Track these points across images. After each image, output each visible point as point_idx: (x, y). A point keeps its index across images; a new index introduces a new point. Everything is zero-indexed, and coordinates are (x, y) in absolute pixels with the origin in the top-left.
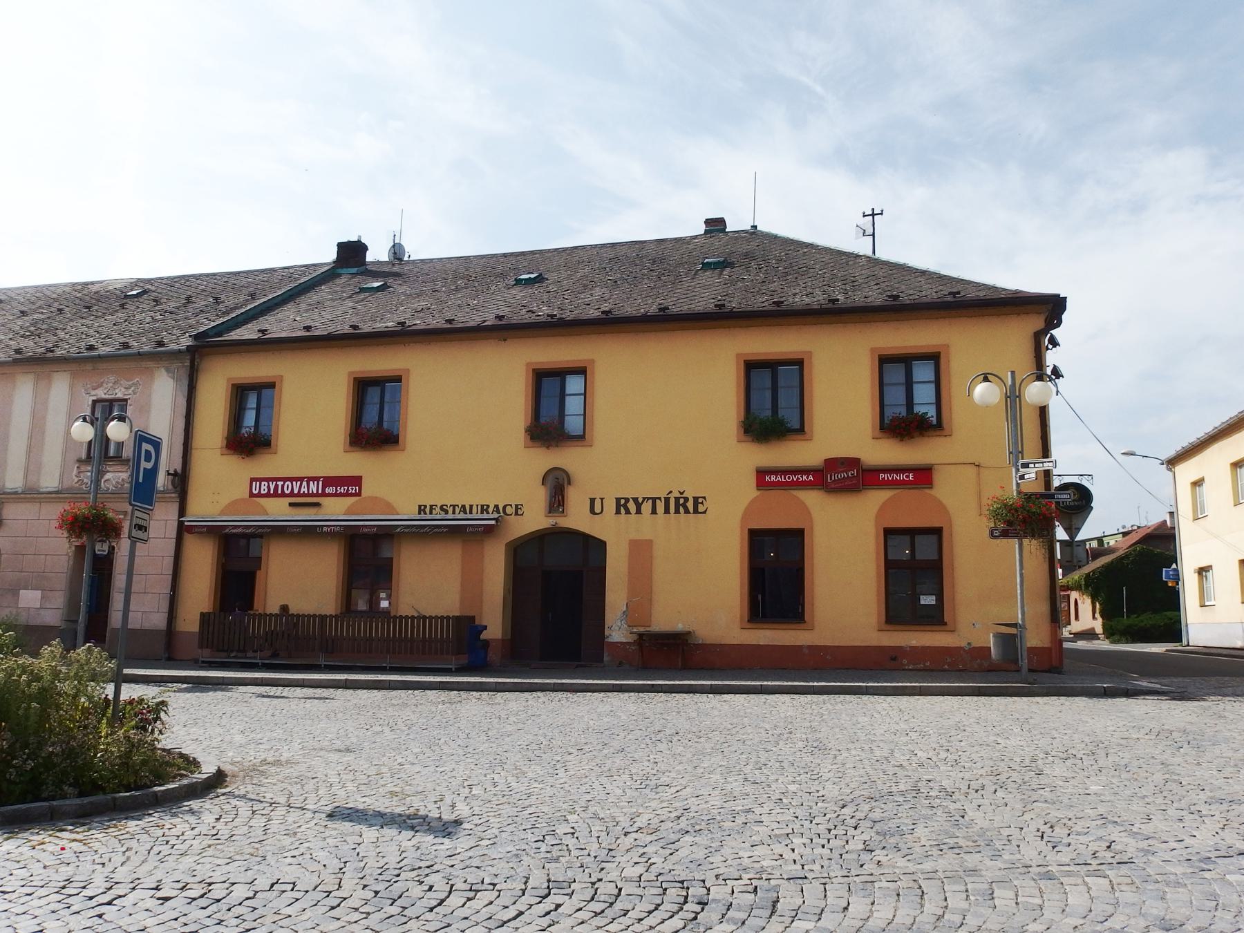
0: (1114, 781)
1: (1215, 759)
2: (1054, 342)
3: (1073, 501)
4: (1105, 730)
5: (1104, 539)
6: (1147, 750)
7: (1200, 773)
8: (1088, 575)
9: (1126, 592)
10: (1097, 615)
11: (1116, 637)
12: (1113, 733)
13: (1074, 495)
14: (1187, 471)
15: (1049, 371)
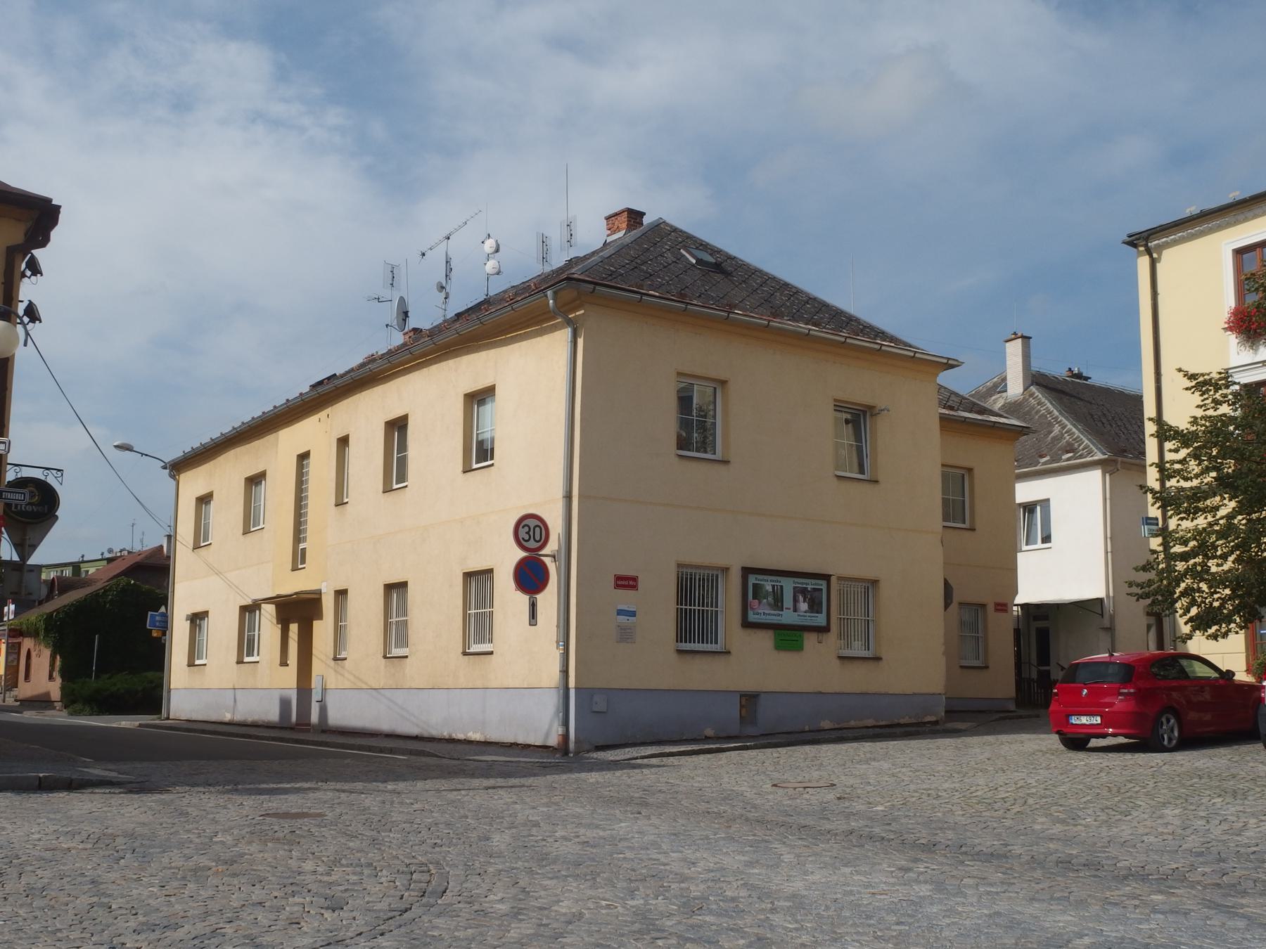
0: (21, 912)
1: (161, 871)
2: (35, 269)
3: (29, 504)
4: (26, 838)
5: (82, 565)
6: (76, 865)
7: (138, 891)
8: (50, 616)
9: (99, 642)
10: (56, 674)
11: (78, 706)
12: (37, 843)
13: (32, 497)
14: (194, 483)
15: (21, 309)
